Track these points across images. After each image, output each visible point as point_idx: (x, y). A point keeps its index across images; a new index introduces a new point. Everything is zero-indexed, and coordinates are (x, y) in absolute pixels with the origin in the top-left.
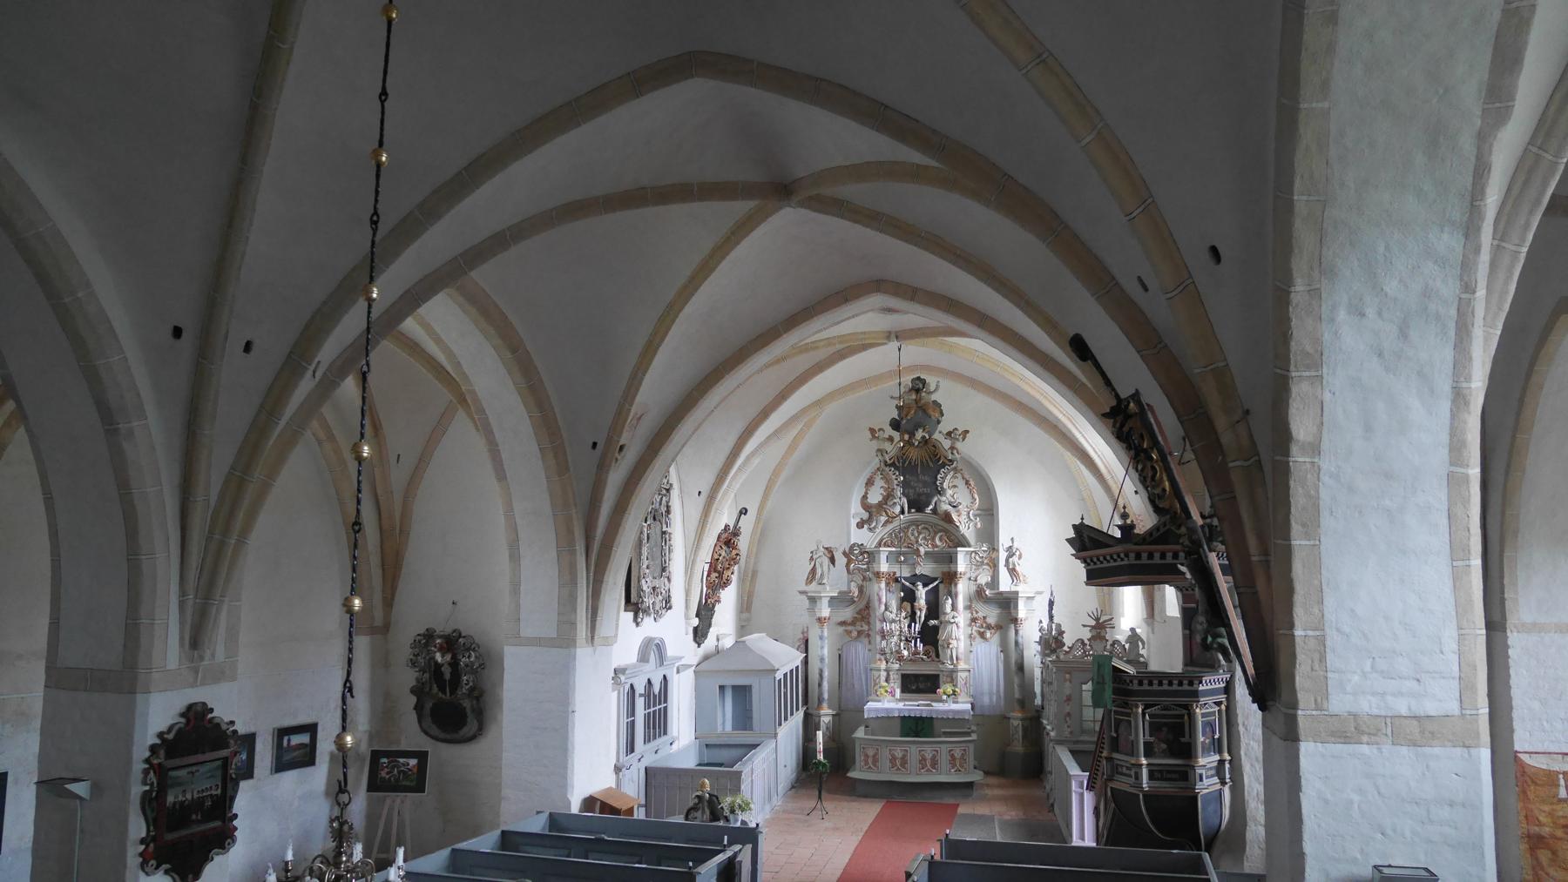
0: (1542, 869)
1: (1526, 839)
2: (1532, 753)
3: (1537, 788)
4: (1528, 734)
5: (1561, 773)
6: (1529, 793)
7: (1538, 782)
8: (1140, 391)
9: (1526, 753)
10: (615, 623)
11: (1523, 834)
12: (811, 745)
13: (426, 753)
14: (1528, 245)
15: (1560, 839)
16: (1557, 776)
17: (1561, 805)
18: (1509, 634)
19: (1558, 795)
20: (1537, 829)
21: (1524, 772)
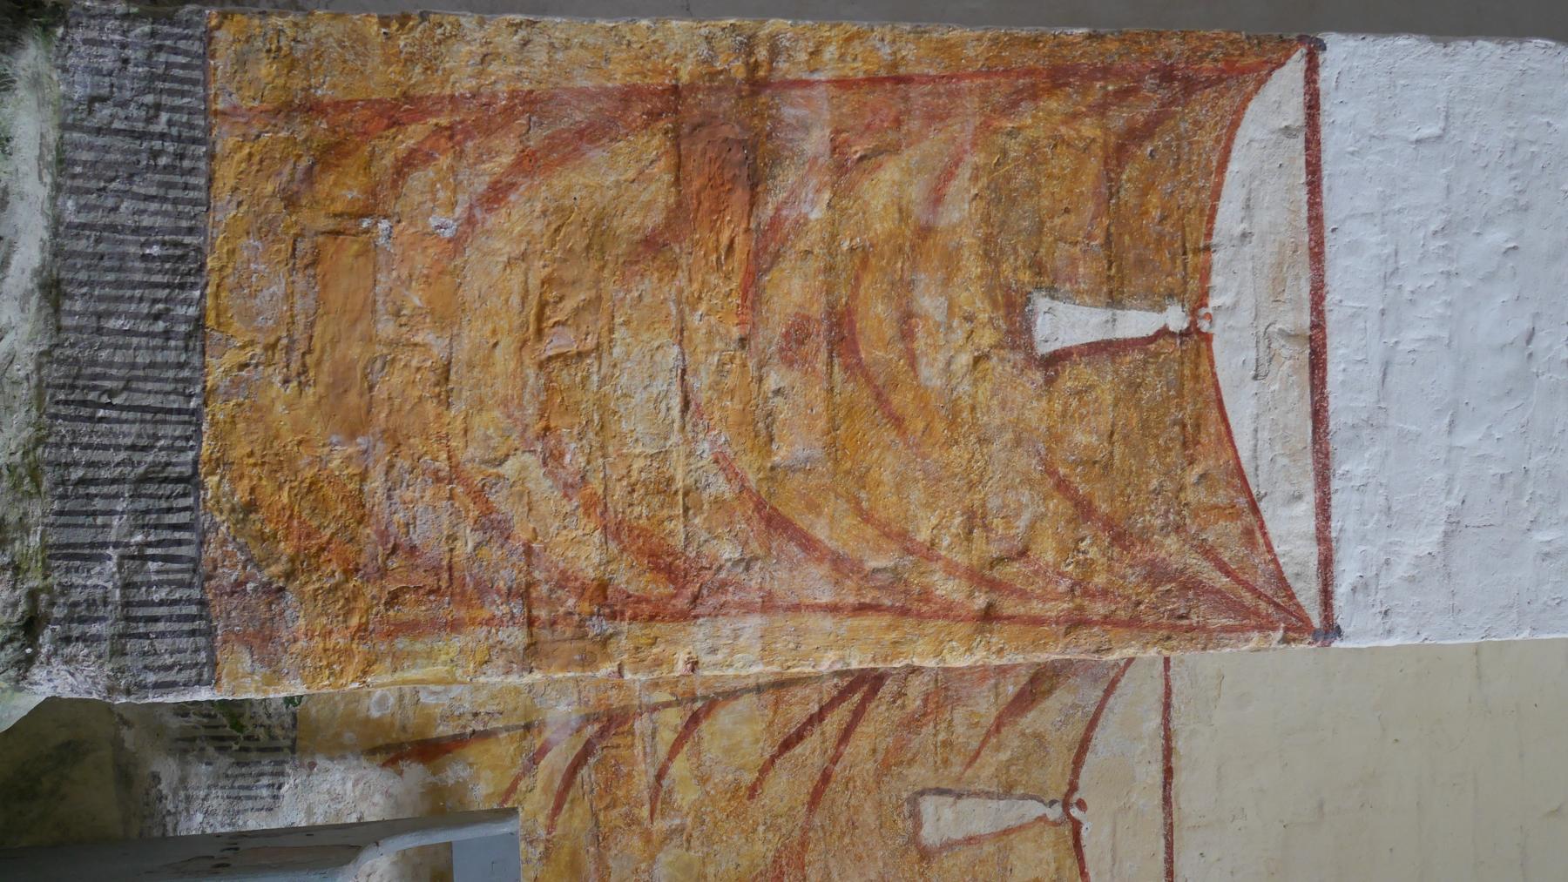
3: (1094, 165)
9: (1313, 106)
15: (752, 292)
19: (1052, 293)
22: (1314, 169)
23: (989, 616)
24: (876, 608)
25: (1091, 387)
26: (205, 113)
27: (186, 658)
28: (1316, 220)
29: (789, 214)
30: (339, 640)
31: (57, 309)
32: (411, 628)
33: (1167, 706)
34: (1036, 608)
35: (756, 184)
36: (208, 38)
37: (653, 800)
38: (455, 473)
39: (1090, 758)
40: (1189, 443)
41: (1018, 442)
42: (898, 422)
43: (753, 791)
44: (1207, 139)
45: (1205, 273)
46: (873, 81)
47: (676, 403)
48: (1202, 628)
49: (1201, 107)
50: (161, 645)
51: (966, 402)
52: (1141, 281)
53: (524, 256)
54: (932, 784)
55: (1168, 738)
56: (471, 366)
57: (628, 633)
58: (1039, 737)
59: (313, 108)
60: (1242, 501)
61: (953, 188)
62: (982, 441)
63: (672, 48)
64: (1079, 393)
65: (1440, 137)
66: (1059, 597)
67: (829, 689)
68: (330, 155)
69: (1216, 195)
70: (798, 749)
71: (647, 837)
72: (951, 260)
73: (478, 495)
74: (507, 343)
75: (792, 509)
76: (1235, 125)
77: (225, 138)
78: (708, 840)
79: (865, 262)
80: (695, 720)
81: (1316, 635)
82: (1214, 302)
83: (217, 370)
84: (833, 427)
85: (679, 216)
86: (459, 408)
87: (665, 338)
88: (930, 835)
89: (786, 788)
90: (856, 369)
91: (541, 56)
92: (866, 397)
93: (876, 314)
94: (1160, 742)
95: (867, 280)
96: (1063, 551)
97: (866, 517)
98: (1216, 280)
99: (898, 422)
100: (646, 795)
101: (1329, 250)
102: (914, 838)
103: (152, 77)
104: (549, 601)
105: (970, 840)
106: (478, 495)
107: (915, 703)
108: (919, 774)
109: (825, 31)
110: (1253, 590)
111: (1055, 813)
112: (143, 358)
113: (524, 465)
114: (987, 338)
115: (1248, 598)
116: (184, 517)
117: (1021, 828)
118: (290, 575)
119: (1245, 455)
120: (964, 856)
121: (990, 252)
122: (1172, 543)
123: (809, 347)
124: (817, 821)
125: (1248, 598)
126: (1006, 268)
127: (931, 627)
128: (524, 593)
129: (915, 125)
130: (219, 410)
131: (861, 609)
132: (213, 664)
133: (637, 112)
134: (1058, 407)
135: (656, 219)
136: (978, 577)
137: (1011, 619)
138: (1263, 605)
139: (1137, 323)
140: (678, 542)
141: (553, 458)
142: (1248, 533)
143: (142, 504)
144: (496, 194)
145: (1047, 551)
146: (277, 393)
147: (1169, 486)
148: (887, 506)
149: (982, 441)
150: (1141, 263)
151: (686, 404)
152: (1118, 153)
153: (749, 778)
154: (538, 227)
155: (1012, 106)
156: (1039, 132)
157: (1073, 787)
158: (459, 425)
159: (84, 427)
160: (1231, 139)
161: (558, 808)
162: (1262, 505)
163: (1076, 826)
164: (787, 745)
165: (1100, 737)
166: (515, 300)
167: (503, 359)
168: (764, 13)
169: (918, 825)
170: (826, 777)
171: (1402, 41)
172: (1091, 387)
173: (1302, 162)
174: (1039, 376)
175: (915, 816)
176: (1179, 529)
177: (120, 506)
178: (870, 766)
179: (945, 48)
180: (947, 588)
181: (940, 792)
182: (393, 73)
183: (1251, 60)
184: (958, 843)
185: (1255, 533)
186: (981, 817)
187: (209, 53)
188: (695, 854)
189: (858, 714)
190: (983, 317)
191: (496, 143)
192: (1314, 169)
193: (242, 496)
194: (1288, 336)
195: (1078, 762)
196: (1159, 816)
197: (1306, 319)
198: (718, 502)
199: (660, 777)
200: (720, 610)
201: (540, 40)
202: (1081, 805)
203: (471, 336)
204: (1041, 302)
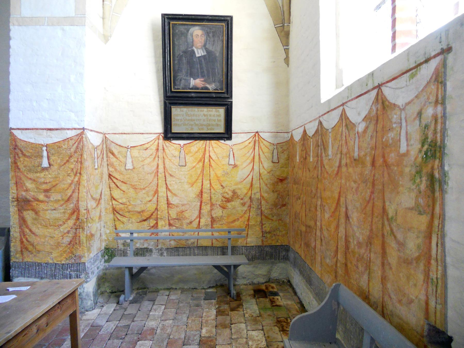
0: (27, 227)
2: (23, 129)
4: (21, 113)
6: (19, 164)
7: (27, 154)
8: (391, 51)
9: (19, 129)
12: (205, 21)
15: (42, 202)
19: (41, 165)
20: (24, 193)
21: (16, 146)
22: (26, 129)
23: (80, 174)
24: (79, 188)
25: (53, 160)
26: (23, 262)
27: (82, 265)
30: (81, 249)
32: (79, 241)
33: (115, 134)
34: (79, 168)
35: (29, 201)
36: (14, 262)
37: (124, 204)
38: (62, 236)
39: (122, 145)
40: (59, 147)
41: (59, 169)
42: (57, 185)
43: (124, 191)
45: (39, 144)
46: (17, 186)
47: (55, 211)
48: (82, 146)
49: (19, 144)
50: (81, 268)
51: (55, 176)
53: (38, 228)
55: (120, 134)
56: (50, 234)
57: (81, 217)
58: (118, 152)
59: (22, 251)
60: (67, 140)
61: (29, 177)
62: (59, 174)
64: (54, 161)
65: (22, 112)
66: (78, 164)
67: (111, 181)
68: (27, 249)
69: (29, 142)
71: (129, 205)
73: (65, 234)
74: (48, 230)
75: (66, 198)
76: (21, 140)
77: (25, 260)
78: (130, 198)
79: (38, 188)
80: (114, 199)
81: (84, 131)
82: (43, 143)
83: (51, 261)
84: (57, 192)
85: (33, 210)
86: (55, 236)
87: (47, 212)
89: (124, 187)
90: (50, 189)
91: (15, 226)
92: (54, 188)
93: (44, 187)
95: (40, 188)
96: (72, 164)
97: (68, 188)
98: (40, 143)
99: (57, 185)
101: (36, 127)
102: (131, 170)
103: (19, 268)
105: (132, 162)
106: (65, 234)
107: (113, 170)
108: (123, 169)
109: (11, 192)
110: (78, 139)
111: (129, 150)
112: (49, 269)
113: (62, 229)
114: (47, 173)
115: (79, 140)
116: (67, 265)
117: (131, 155)
118: (74, 254)
121: (36, 172)
122: (72, 150)
123: (48, 195)
124: (128, 183)
125: (79, 140)
127: (81, 181)
128: (76, 229)
129: (21, 181)
130: (55, 262)
132: (83, 263)
134: (55, 164)
135: (33, 213)
136: (75, 175)
138: (80, 138)
139: (45, 154)
140: (71, 211)
141: (61, 225)
142: (71, 139)
143: (65, 270)
144: (31, 231)
145: (72, 166)
146: (53, 255)
149: (59, 174)
151: (55, 210)
152: (24, 155)
153: (122, 192)
154: (35, 226)
156: (22, 165)
157: (126, 147)
158: (57, 236)
159: (57, 275)
161: (125, 217)
162: (68, 138)
163: (131, 147)
164: (118, 187)
165: (119, 143)
166: (43, 229)
167: (50, 231)
168: (9, 200)
169: (130, 169)
170: (122, 182)
172: (53, 160)
173: (25, 131)
174: (52, 167)
175: (128, 170)
177: (65, 272)
178: (121, 176)
179: (12, 177)
180: (76, 179)
181: (125, 166)
183: (13, 138)
185: (71, 139)
186: (129, 161)
187: (16, 262)
189: (114, 177)
190: (44, 173)
191: (25, 231)
192: (26, 129)
193: (65, 259)
194: (47, 133)
195: (122, 147)
196: (130, 135)
197: (45, 131)
199: (121, 203)
200: (78, 206)
202: (128, 146)
204: (43, 166)
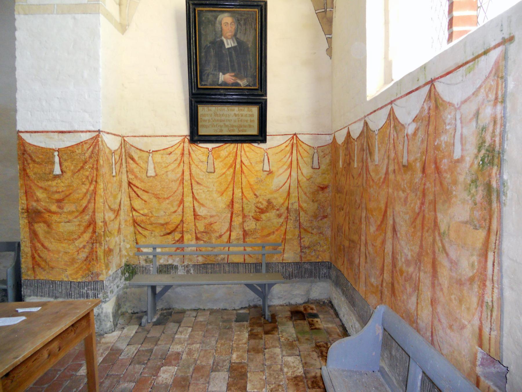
1: (26, 214)
3: (36, 165)
5: (55, 151)
6: (28, 171)
7: (37, 160)
9: (27, 132)
10: (281, 190)
11: (23, 209)
13: (264, 141)
14: (164, 251)
15: (54, 213)
16: (53, 154)
17: (56, 181)
18: (16, 16)
19: (53, 172)
20: (34, 204)
21: (25, 151)
22: (35, 132)
23: (96, 182)
28: (42, 132)
29: (44, 208)
30: (98, 266)
31: (59, 297)
32: (97, 257)
33: (135, 136)
34: (95, 175)
36: (26, 279)
42: (70, 194)
43: (145, 201)
44: (32, 148)
46: (26, 196)
49: (28, 148)
52: (51, 159)
54: (145, 174)
55: (140, 136)
56: (64, 249)
57: (97, 230)
58: (139, 157)
59: (33, 267)
60: (81, 144)
63: (23, 223)
64: (66, 168)
67: (130, 190)
68: (39, 265)
69: (39, 147)
70: (139, 195)
71: (151, 217)
72: (49, 186)
75: (81, 209)
76: (30, 144)
77: (38, 278)
79: (50, 198)
80: (135, 210)
83: (66, 279)
85: (45, 222)
88: (153, 174)
89: (145, 196)
92: (67, 198)
93: (57, 196)
94: (141, 137)
96: (87, 171)
97: (83, 198)
98: (51, 147)
99: (70, 194)
100: (145, 217)
102: (153, 177)
104: (94, 240)
105: (155, 168)
106: (80, 249)
108: (144, 176)
109: (20, 202)
110: (93, 143)
111: (151, 155)
113: (77, 243)
114: (59, 181)
118: (90, 272)
119: (75, 143)
120: (157, 169)
121: (48, 180)
122: (87, 155)
123: (61, 206)
125: (94, 144)
126: (50, 178)
127: (97, 190)
131: (95, 199)
132: (101, 281)
133: (32, 228)
135: (45, 225)
136: (91, 183)
137: (96, 178)
139: (57, 159)
140: (86, 223)
141: (76, 239)
142: (85, 143)
144: (43, 245)
147: (79, 155)
148: (81, 196)
150: (49, 158)
153: (143, 202)
155: (29, 177)
157: (147, 152)
160: (32, 145)
163: (153, 151)
164: (139, 196)
167: (64, 245)
170: (144, 190)
171: (17, 118)
175: (151, 177)
176: (85, 154)
177: (82, 291)
180: (92, 187)
181: (147, 173)
182: (29, 258)
184: (155, 170)
185: (85, 142)
186: (151, 167)
188: (154, 210)
189: (134, 185)
192: (35, 132)
195: (143, 151)
196: (152, 138)
198: (81, 218)
201: (23, 240)
202: (150, 151)
203: (61, 249)
204: (55, 173)
